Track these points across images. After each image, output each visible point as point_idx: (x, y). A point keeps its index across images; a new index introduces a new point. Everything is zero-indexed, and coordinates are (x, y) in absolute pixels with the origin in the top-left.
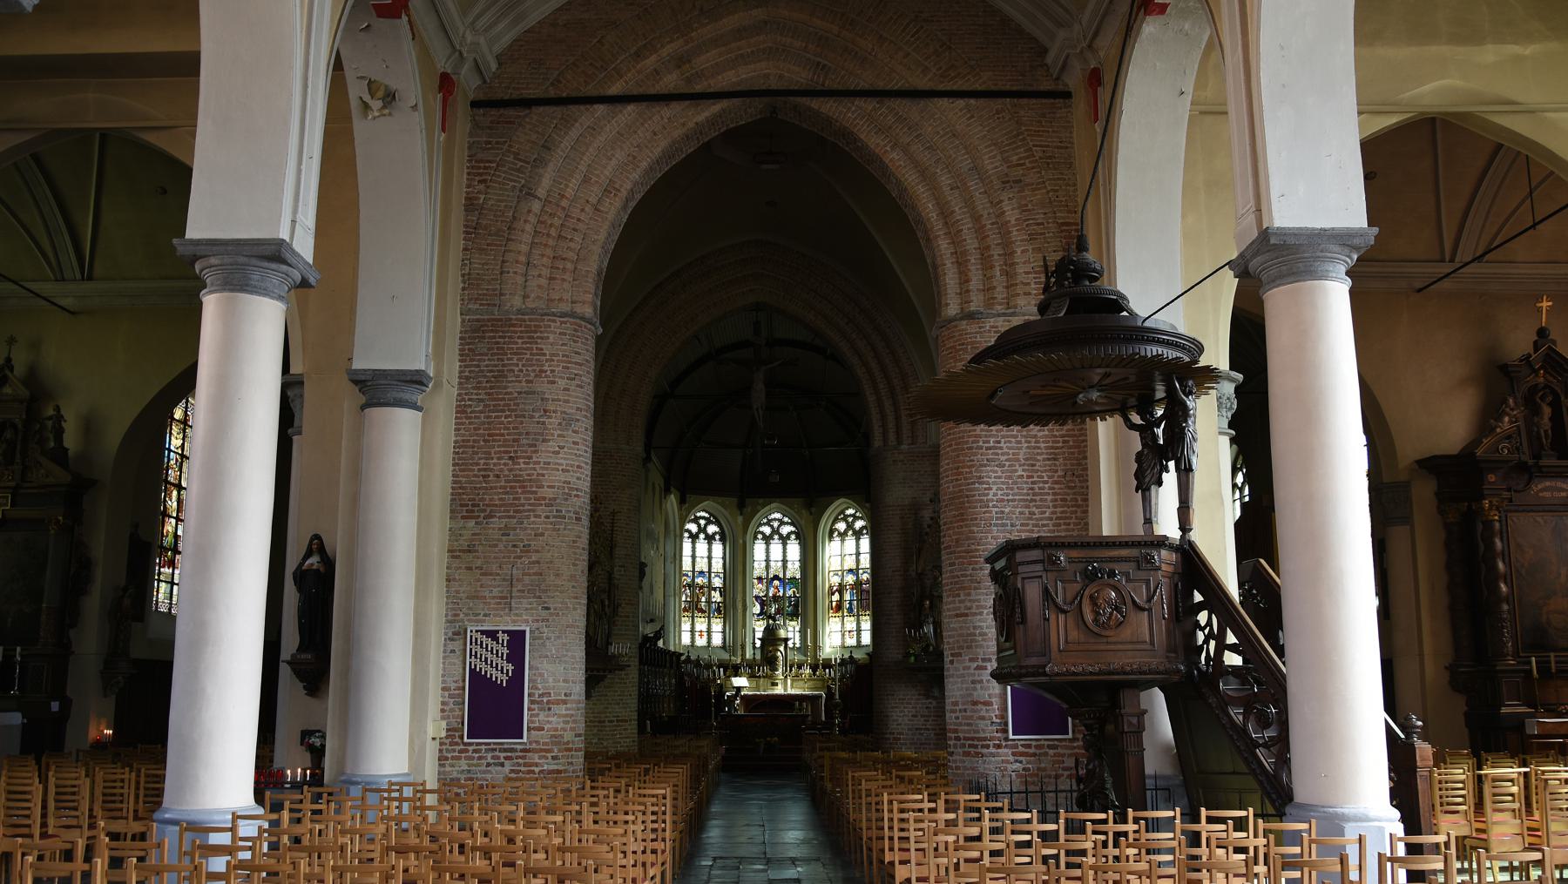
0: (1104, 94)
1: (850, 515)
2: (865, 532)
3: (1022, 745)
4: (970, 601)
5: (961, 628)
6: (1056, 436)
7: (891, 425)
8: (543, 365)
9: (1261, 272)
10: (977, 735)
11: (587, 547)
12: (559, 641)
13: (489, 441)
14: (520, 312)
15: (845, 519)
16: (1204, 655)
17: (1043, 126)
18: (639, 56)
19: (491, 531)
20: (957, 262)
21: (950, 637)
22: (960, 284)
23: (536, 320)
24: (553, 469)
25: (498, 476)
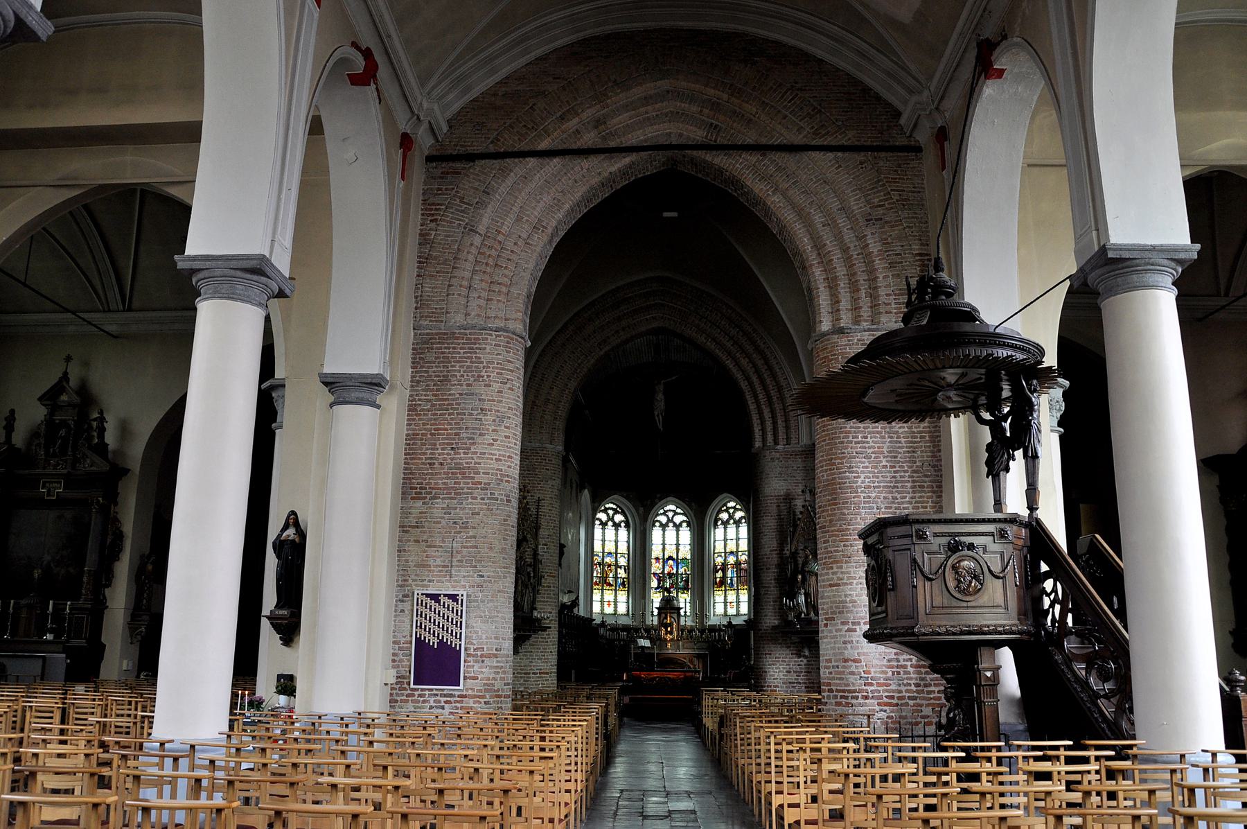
0: (950, 148)
1: (732, 508)
2: (743, 521)
3: (886, 697)
4: (842, 572)
5: (834, 596)
6: (914, 432)
7: (769, 428)
8: (481, 371)
9: (1097, 286)
10: (847, 688)
11: (516, 525)
12: (492, 604)
13: (434, 434)
14: (460, 327)
15: (727, 511)
16: (1050, 617)
17: (899, 175)
18: (563, 119)
19: (435, 510)
20: (829, 286)
21: (824, 603)
22: (832, 304)
23: (475, 334)
24: (487, 459)
25: (441, 464)
